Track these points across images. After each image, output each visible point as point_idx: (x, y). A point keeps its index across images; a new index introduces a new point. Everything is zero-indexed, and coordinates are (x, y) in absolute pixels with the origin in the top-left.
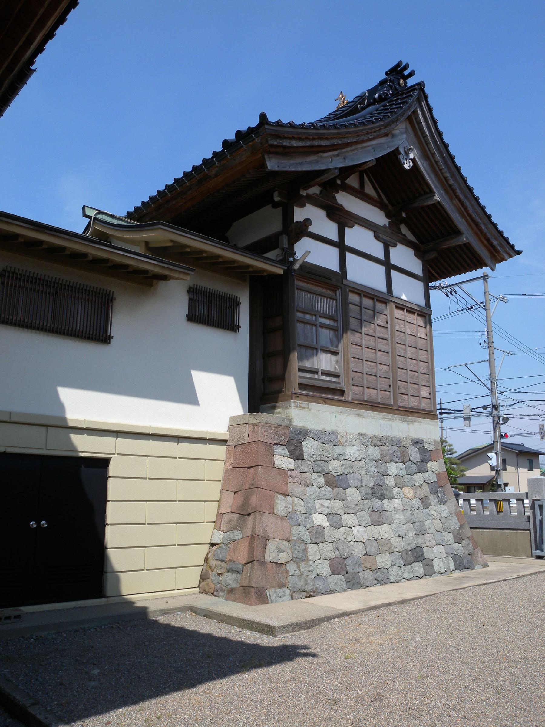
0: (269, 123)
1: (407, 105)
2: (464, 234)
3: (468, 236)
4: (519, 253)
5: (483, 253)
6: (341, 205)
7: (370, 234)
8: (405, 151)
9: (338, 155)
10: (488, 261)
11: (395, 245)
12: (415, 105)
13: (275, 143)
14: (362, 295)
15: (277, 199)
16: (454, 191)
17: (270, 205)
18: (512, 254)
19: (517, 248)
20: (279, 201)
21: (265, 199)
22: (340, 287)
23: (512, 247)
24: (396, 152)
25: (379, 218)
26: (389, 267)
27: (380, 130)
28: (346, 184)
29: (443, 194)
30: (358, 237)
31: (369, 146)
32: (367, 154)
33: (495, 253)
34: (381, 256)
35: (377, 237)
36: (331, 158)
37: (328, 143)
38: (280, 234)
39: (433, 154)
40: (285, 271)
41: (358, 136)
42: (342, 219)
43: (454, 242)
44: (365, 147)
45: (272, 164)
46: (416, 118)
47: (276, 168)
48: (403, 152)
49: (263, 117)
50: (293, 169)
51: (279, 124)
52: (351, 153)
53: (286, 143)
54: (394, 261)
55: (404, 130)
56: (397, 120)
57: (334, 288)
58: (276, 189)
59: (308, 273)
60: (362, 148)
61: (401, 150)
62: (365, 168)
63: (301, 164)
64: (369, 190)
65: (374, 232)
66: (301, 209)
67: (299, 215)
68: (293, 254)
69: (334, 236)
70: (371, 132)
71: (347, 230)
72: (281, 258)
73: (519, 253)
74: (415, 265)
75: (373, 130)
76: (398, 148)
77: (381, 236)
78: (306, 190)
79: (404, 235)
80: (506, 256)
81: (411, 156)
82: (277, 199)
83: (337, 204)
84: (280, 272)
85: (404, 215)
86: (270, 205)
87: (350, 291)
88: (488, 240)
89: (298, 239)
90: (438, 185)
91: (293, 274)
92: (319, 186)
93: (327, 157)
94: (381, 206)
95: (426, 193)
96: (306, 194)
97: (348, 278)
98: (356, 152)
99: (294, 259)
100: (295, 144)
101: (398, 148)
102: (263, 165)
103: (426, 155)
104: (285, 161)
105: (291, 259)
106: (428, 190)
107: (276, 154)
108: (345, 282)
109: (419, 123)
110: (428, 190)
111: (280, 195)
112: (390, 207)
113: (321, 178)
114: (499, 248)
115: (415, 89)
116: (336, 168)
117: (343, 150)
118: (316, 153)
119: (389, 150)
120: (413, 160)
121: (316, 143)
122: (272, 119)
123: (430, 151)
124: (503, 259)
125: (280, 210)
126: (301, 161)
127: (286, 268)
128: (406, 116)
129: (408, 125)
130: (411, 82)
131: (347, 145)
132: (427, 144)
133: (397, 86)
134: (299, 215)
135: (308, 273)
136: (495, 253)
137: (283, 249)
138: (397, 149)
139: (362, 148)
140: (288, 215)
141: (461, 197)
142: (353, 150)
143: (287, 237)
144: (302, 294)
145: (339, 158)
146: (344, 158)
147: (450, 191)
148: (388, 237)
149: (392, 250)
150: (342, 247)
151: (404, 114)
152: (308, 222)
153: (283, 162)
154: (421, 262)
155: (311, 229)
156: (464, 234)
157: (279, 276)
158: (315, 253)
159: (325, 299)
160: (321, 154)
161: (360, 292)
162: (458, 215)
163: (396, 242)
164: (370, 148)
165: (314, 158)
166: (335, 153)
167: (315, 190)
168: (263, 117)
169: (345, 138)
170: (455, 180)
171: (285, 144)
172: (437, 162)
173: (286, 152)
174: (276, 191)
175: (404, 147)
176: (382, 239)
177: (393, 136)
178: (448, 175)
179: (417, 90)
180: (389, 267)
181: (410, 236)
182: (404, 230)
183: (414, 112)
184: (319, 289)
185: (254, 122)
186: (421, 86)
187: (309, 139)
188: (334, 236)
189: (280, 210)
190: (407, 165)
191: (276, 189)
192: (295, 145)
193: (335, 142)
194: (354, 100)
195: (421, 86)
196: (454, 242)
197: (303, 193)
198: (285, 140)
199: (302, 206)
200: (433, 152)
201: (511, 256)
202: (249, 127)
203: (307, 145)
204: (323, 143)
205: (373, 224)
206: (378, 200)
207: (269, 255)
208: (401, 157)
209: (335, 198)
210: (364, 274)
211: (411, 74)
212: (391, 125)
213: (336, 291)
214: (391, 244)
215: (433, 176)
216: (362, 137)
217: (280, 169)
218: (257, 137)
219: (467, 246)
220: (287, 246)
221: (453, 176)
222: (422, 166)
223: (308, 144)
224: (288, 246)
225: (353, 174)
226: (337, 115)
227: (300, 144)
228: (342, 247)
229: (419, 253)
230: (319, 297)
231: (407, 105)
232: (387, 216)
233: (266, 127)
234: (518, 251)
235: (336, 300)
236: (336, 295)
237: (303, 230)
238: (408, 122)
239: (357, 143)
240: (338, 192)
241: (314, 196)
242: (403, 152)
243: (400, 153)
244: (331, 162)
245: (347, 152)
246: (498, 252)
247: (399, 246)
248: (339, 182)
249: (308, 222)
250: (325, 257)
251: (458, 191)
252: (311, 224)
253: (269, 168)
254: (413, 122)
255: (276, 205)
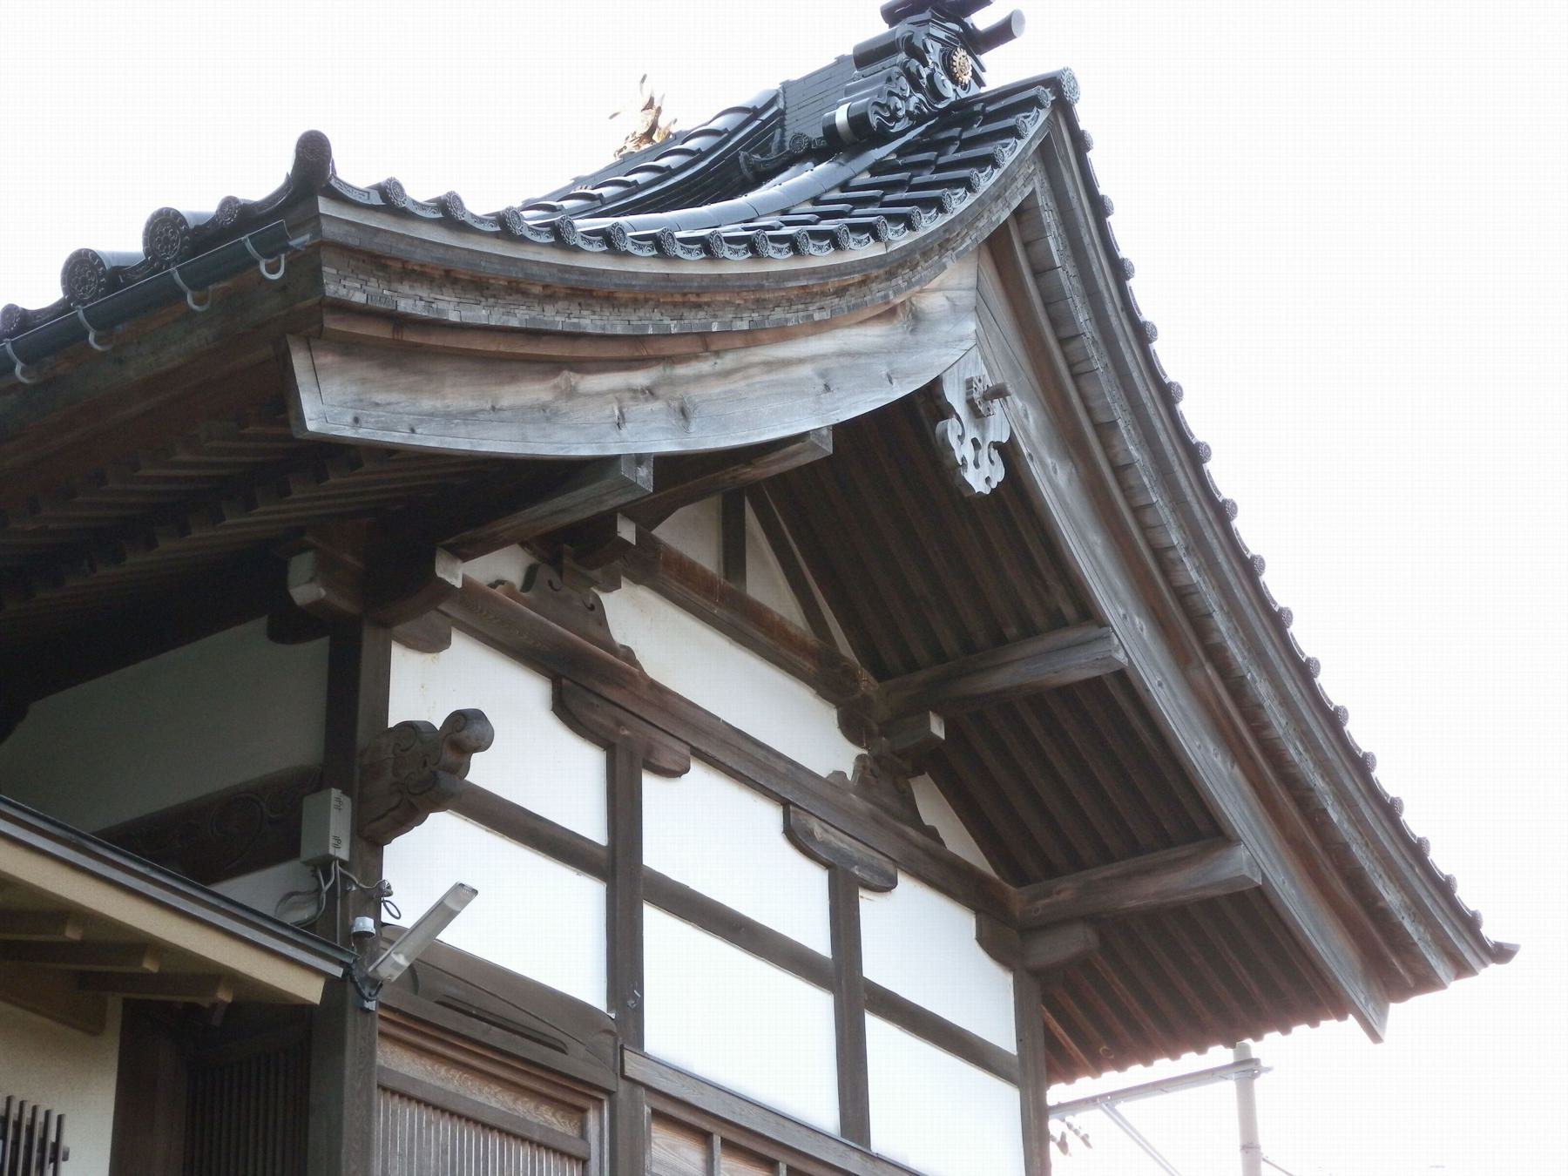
0: (338, 196)
1: (997, 173)
2: (1239, 841)
3: (1256, 855)
4: (1501, 953)
5: (1330, 945)
6: (628, 654)
7: (769, 816)
8: (971, 403)
9: (650, 392)
10: (1355, 990)
11: (885, 885)
12: (1028, 179)
13: (359, 298)
14: (717, 1141)
15: (305, 592)
16: (1200, 623)
17: (259, 625)
18: (1469, 956)
19: (1491, 931)
20: (318, 603)
21: (239, 590)
22: (609, 1093)
23: (1470, 924)
24: (926, 405)
25: (813, 738)
26: (856, 998)
27: (863, 283)
28: (655, 541)
29: (1145, 634)
30: (703, 829)
31: (801, 361)
32: (788, 397)
33: (1386, 951)
34: (817, 938)
35: (796, 836)
36: (620, 401)
37: (616, 324)
38: (314, 781)
39: (1106, 430)
40: (331, 983)
41: (760, 304)
42: (631, 726)
43: (1184, 880)
44: (786, 363)
45: (330, 403)
46: (1026, 245)
47: (343, 429)
48: (960, 407)
49: (313, 155)
50: (433, 443)
51: (389, 199)
52: (716, 389)
53: (410, 301)
54: (878, 967)
55: (968, 298)
56: (942, 243)
57: (574, 1094)
58: (308, 538)
59: (448, 1004)
60: (771, 366)
61: (954, 396)
62: (775, 469)
63: (469, 416)
64: (768, 586)
65: (786, 804)
66: (428, 657)
67: (423, 686)
68: (376, 896)
69: (586, 817)
70: (824, 294)
71: (652, 787)
72: (305, 914)
73: (1501, 953)
74: (984, 1000)
75: (833, 283)
76: (937, 383)
77: (817, 829)
78: (465, 558)
79: (932, 833)
80: (1441, 968)
81: (998, 431)
82: (305, 592)
83: (609, 645)
84: (310, 990)
85: (938, 729)
86: (259, 625)
87: (658, 1115)
88: (1357, 881)
89: (407, 816)
90: (1118, 583)
91: (371, 1005)
92: (523, 544)
93: (600, 394)
94: (827, 679)
95: (1058, 622)
96: (465, 579)
97: (649, 1046)
98: (737, 384)
99: (380, 925)
100: (453, 309)
101: (937, 383)
102: (284, 401)
103: (1074, 433)
104: (393, 397)
105: (367, 924)
106: (1069, 611)
107: (351, 348)
108: (633, 1067)
109: (1042, 270)
110: (1069, 611)
111: (326, 569)
112: (867, 683)
113: (560, 502)
114: (1408, 925)
115: (1035, 102)
116: (639, 459)
117: (682, 370)
118: (554, 366)
119: (899, 392)
120: (1008, 452)
121: (555, 317)
122: (355, 168)
123: (1089, 410)
124: (1426, 981)
125: (316, 650)
126: (472, 405)
127: (338, 972)
128: (985, 227)
129: (989, 272)
130: (1001, 69)
131: (705, 344)
132: (1075, 377)
133: (941, 77)
134: (423, 686)
135: (448, 1004)
136: (1386, 951)
137: (324, 865)
138: (933, 390)
139: (771, 366)
140: (353, 686)
141: (1237, 652)
142: (726, 374)
143: (347, 801)
144: (409, 1116)
145: (656, 406)
146: (684, 413)
147: (1181, 624)
148: (853, 840)
149: (870, 906)
150: (623, 875)
151: (978, 218)
152: (467, 731)
153: (379, 397)
154: (1009, 979)
155: (483, 772)
156: (1239, 841)
157: (300, 1009)
158: (482, 898)
159: (525, 1151)
160: (575, 378)
161: (707, 1126)
162: (1211, 747)
163: (890, 868)
164: (806, 371)
165: (535, 391)
166: (640, 378)
167: (501, 567)
168: (313, 155)
169: (698, 306)
170: (1210, 566)
171: (405, 306)
172: (1120, 470)
173: (404, 346)
174: (302, 549)
175: (969, 383)
176: (825, 845)
177: (916, 318)
178: (1175, 538)
179: (1041, 106)
180: (856, 998)
181: (960, 843)
182: (933, 809)
183: (1018, 213)
184: (492, 1099)
185: (262, 176)
186: (1054, 94)
187: (525, 294)
188: (586, 817)
189: (316, 650)
190: (982, 476)
191: (308, 538)
192: (453, 317)
193: (650, 321)
194: (718, 124)
195: (1054, 94)
196: (1184, 880)
197: (453, 573)
198: (405, 288)
199: (434, 643)
200: (1103, 418)
201: (1462, 968)
202: (229, 203)
203: (514, 323)
204: (590, 322)
205: (781, 766)
206: (811, 639)
207: (238, 888)
208: (951, 429)
209: (596, 609)
210: (732, 1028)
211: (1003, 33)
212: (913, 268)
213: (583, 1111)
214: (866, 876)
215: (1096, 539)
216: (778, 314)
217: (364, 433)
218: (268, 256)
219: (1254, 903)
220: (343, 853)
221: (1198, 543)
222: (1054, 481)
223: (519, 317)
224: (351, 855)
225: (684, 503)
226: (636, 187)
227: (480, 314)
228: (623, 875)
229: (1001, 938)
230: (494, 1141)
231: (997, 173)
232: (852, 727)
233: (325, 206)
234: (1499, 946)
235: (584, 1161)
236: (583, 1134)
237: (430, 773)
238: (986, 256)
239: (751, 338)
240: (613, 585)
241: (498, 592)
242: (960, 407)
243: (946, 411)
244: (610, 421)
245: (699, 378)
246: (1401, 944)
247: (907, 886)
248: (627, 532)
249: (467, 731)
250: (530, 925)
251: (1220, 621)
252: (483, 743)
253: (311, 426)
254: (1015, 262)
255: (292, 625)
